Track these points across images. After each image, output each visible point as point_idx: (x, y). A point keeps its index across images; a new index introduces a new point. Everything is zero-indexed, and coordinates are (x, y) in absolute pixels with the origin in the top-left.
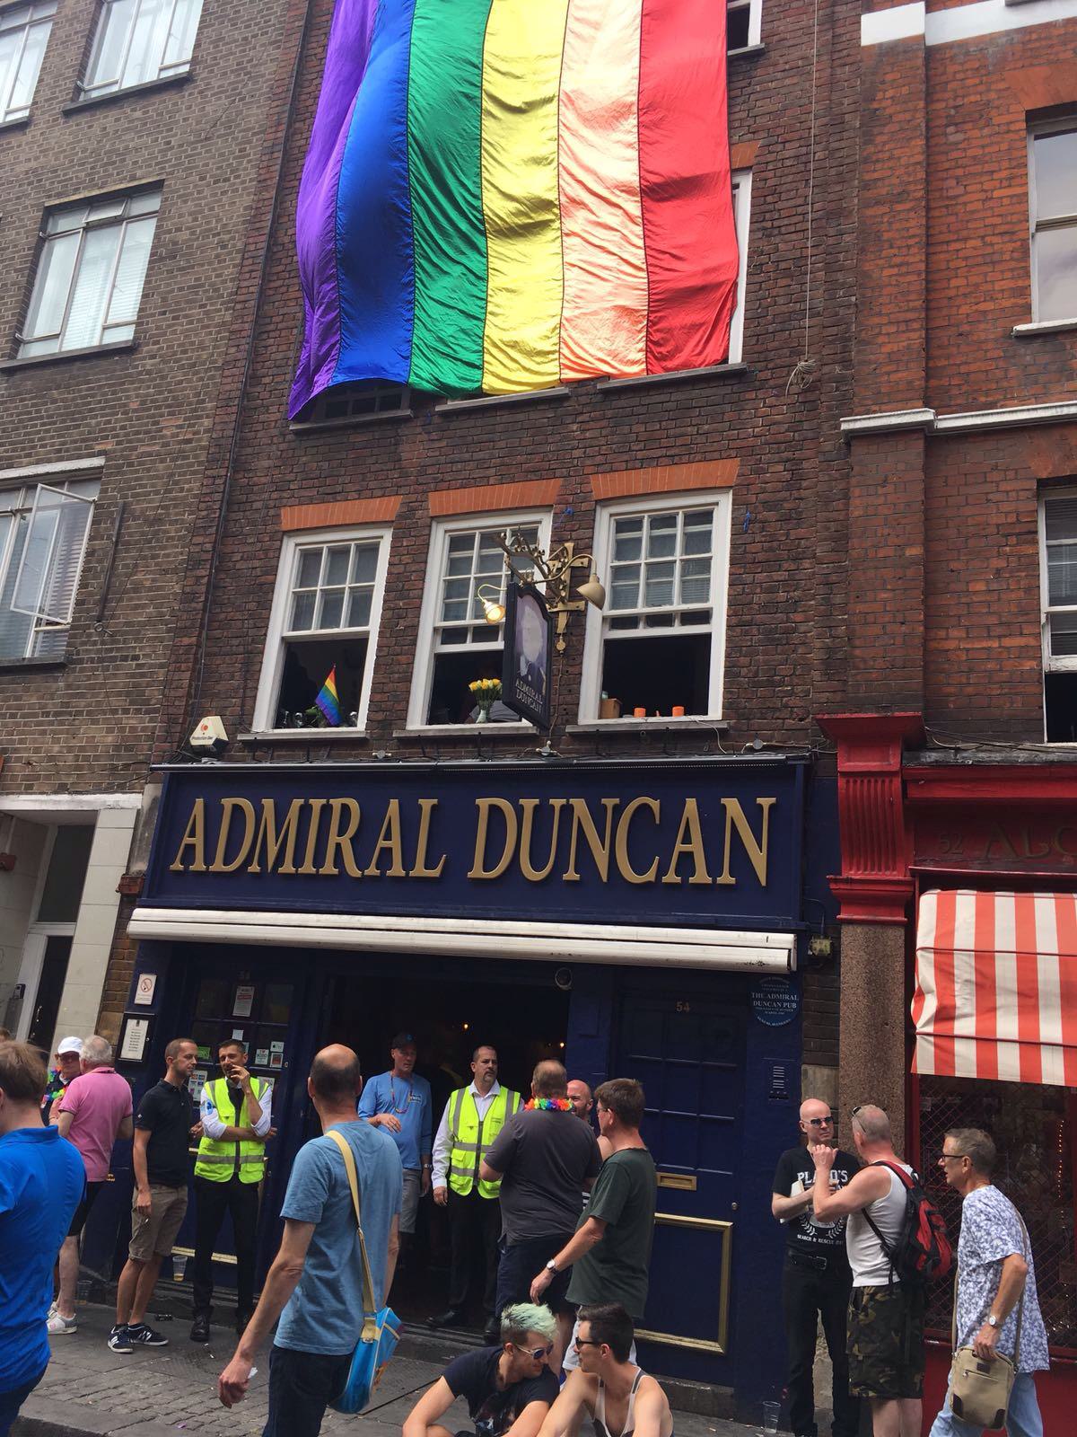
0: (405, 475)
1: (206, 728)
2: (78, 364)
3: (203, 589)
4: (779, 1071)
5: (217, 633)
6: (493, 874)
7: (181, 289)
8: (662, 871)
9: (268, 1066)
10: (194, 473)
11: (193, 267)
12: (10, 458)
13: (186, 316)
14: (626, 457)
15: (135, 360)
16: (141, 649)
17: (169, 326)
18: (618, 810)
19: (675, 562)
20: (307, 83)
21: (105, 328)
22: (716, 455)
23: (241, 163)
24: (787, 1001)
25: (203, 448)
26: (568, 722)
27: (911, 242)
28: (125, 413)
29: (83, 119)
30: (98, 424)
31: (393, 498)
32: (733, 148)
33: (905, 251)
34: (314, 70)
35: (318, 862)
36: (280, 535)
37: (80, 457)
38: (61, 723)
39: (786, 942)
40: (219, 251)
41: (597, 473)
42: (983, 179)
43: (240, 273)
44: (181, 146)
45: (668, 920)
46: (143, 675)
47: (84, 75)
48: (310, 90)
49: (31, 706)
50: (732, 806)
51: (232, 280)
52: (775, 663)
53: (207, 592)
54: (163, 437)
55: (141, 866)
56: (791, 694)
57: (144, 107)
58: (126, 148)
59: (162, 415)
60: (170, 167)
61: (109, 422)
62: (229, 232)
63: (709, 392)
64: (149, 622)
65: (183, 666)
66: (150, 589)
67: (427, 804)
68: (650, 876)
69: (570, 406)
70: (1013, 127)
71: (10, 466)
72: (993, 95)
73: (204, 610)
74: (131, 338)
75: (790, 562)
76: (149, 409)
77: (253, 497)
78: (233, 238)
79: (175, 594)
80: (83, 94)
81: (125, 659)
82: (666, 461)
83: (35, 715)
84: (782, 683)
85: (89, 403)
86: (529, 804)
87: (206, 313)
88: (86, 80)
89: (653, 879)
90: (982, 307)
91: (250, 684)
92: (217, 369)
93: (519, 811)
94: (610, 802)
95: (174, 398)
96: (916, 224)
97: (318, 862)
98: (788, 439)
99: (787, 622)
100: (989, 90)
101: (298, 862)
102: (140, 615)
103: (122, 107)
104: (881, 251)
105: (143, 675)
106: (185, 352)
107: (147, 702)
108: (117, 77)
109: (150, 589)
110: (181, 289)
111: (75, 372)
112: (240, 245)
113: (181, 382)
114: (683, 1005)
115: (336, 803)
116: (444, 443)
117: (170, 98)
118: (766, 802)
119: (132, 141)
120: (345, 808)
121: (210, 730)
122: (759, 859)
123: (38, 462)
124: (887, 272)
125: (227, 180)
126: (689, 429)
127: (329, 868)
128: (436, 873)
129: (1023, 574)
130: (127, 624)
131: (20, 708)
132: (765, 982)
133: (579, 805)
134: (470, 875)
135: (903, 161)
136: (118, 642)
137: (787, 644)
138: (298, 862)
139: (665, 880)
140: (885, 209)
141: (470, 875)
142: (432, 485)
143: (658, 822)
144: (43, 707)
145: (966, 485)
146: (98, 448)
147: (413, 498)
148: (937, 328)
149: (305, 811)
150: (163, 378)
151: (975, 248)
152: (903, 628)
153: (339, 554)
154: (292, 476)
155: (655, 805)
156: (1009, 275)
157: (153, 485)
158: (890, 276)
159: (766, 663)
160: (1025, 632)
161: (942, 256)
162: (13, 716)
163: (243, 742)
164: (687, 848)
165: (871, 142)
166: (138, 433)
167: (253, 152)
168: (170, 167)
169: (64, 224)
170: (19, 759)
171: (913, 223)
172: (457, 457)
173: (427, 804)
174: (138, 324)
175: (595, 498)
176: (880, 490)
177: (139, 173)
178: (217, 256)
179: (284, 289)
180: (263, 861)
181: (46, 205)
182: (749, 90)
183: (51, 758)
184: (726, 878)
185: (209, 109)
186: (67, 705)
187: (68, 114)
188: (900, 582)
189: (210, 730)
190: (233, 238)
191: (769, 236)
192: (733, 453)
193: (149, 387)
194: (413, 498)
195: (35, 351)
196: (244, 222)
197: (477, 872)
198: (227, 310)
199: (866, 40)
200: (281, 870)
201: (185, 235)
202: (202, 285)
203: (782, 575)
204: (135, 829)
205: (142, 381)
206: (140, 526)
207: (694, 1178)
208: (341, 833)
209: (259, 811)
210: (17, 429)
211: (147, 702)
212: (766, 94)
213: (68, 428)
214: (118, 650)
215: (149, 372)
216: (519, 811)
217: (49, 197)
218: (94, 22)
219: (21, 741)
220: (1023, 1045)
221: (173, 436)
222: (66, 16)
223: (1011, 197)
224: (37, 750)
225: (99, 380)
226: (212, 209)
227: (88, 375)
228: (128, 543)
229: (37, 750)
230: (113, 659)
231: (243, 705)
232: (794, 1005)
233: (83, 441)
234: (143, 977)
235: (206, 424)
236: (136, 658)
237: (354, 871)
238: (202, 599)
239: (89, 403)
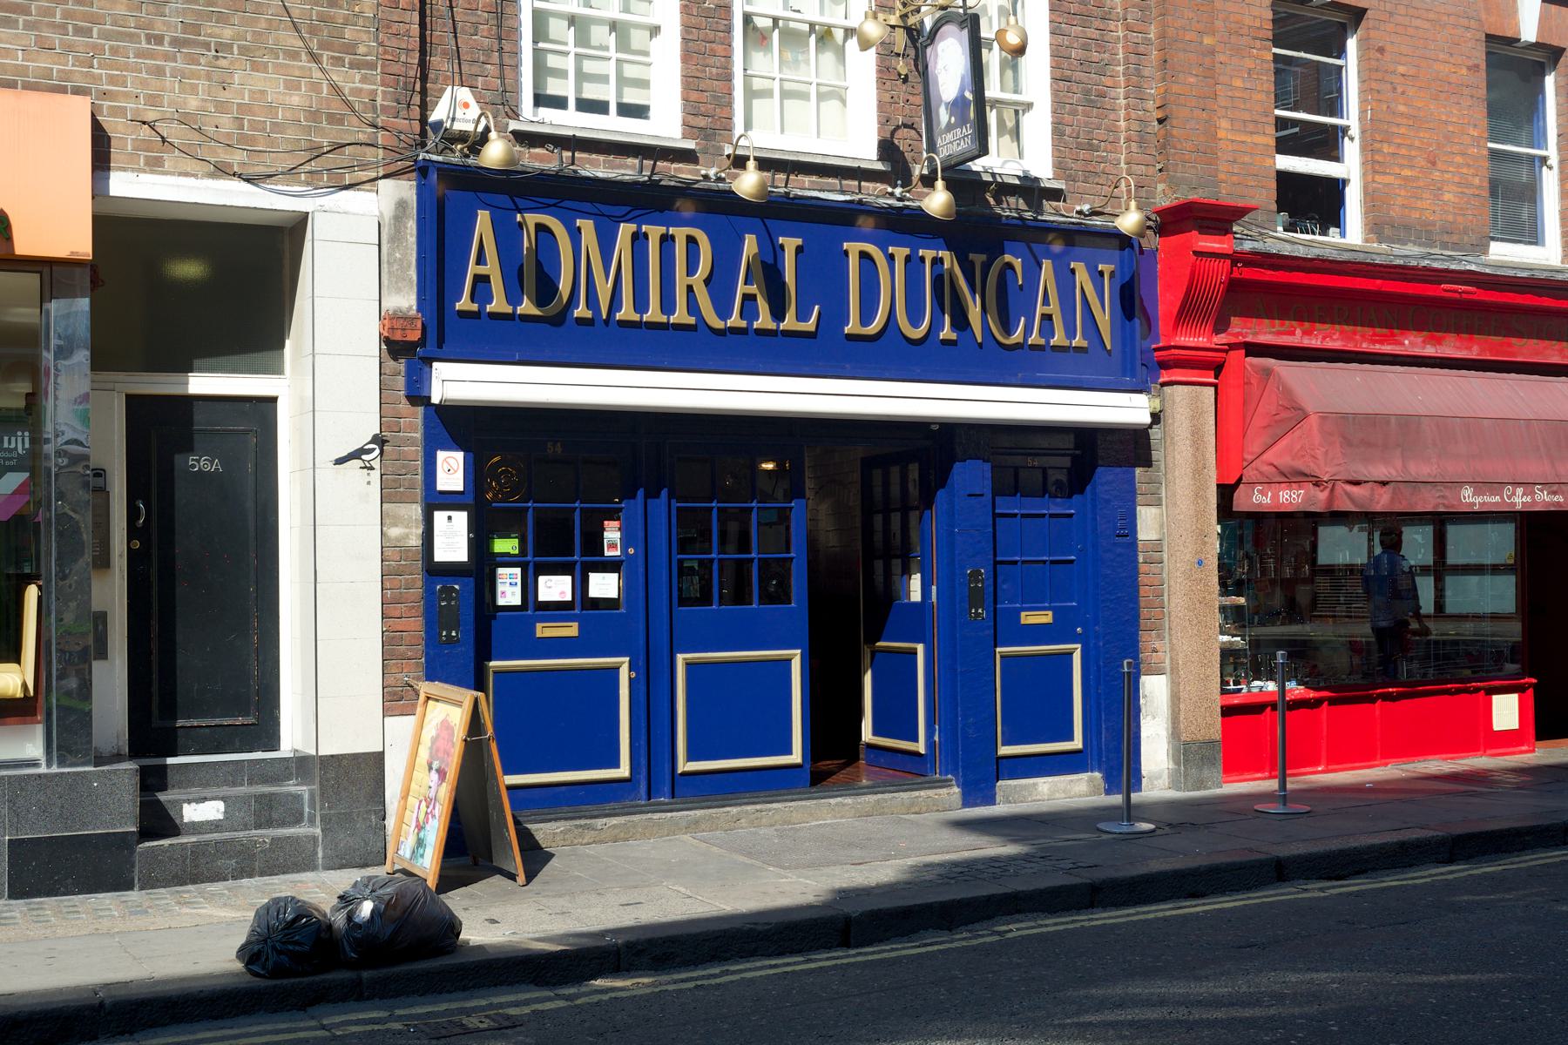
8: (1028, 330)
35: (667, 305)
52: (1093, 126)
86: (901, 253)
91: (507, 46)
93: (891, 258)
97: (667, 305)
101: (640, 303)
107: (350, 48)
120: (691, 240)
127: (680, 315)
128: (810, 325)
138: (640, 303)
160: (808, 25)
164: (482, 270)
170: (122, 112)
173: (790, 244)
180: (592, 301)
184: (1078, 341)
186: (196, 28)
197: (852, 326)
200: (618, 316)
207: (1050, 613)
209: (575, 234)
211: (350, 48)
231: (502, 77)
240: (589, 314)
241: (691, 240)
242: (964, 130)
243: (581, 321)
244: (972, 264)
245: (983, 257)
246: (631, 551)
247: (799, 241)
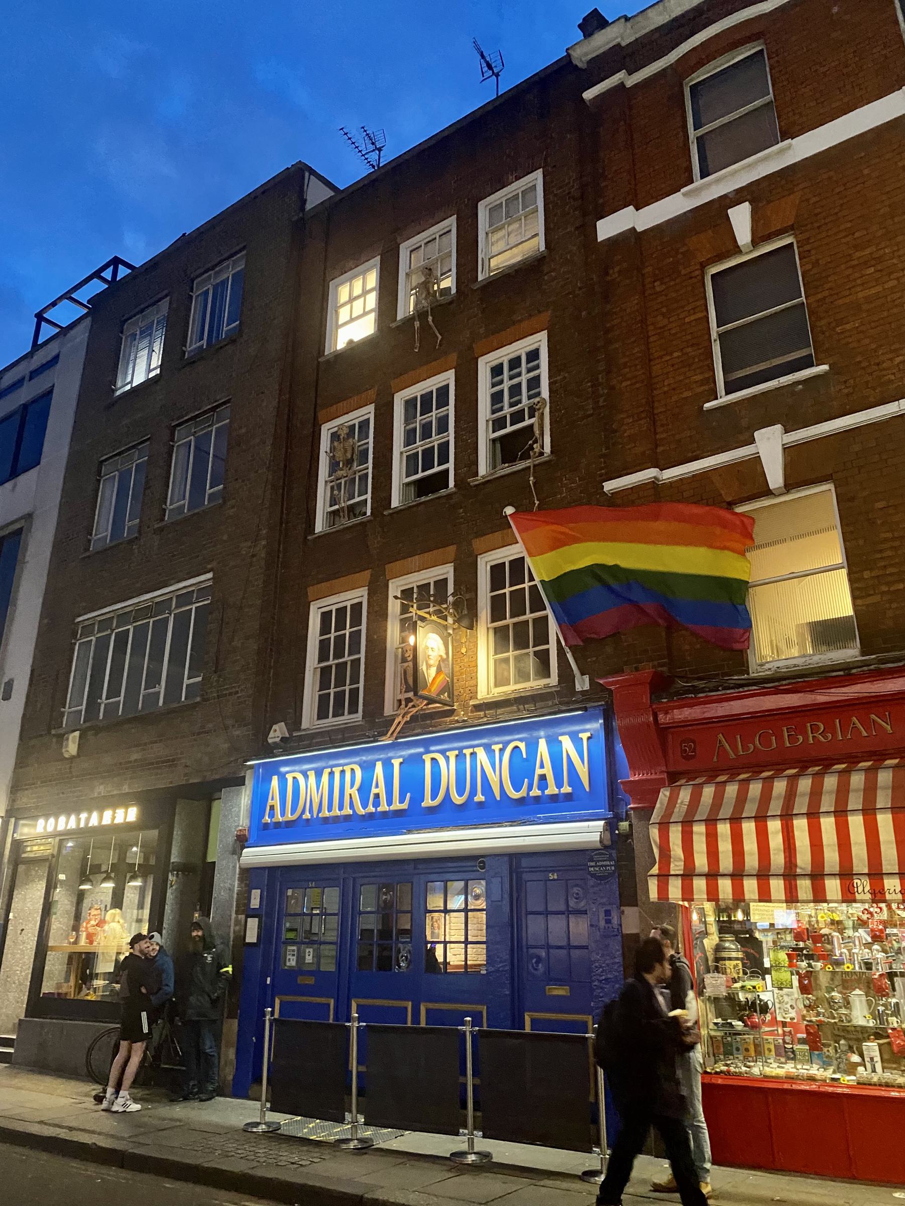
1: (275, 731)
6: (436, 802)
8: (530, 788)
18: (502, 751)
24: (608, 866)
26: (471, 698)
27: (637, 362)
32: (66, 302)
33: (633, 368)
39: (599, 826)
42: (679, 311)
70: (693, 275)
72: (680, 256)
81: (230, 694)
89: (525, 795)
114: (553, 875)
120: (352, 770)
124: (624, 384)
127: (348, 811)
128: (404, 806)
132: (596, 855)
134: (423, 805)
135: (628, 311)
139: (532, 794)
141: (423, 805)
146: (209, 566)
155: (522, 746)
156: (698, 371)
158: (626, 386)
171: (636, 350)
180: (311, 811)
184: (567, 789)
197: (428, 802)
199: (601, 237)
200: (320, 815)
201: (243, 430)
219: (182, 753)
220: (710, 878)
223: (696, 320)
232: (613, 868)
234: (254, 891)
241: (352, 770)
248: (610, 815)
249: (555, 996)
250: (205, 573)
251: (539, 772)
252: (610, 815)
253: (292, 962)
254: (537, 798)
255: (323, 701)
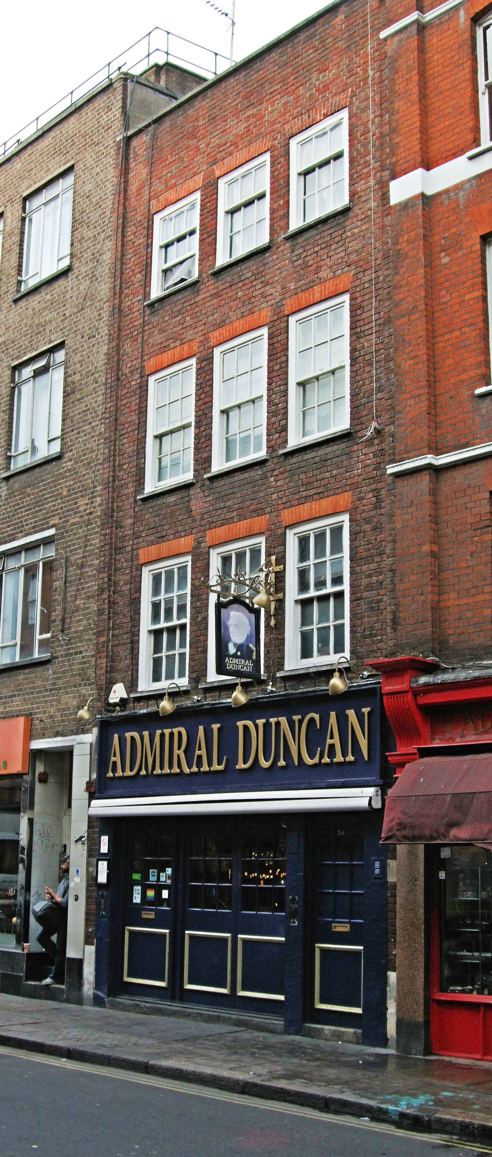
0: (194, 521)
1: (115, 692)
2: (37, 470)
3: (106, 606)
4: (377, 864)
5: (117, 632)
6: (133, 773)
7: (79, 414)
8: (321, 757)
9: (166, 881)
10: (96, 533)
11: (83, 398)
12: (13, 534)
13: (83, 431)
14: (297, 497)
15: (63, 463)
16: (83, 646)
17: (76, 439)
18: (301, 722)
19: (326, 561)
20: (128, 261)
21: (50, 441)
22: (340, 490)
23: (99, 324)
25: (98, 517)
28: (61, 499)
29: (23, 303)
30: (50, 507)
31: (190, 536)
34: (131, 251)
36: (140, 566)
37: (44, 530)
38: (53, 695)
40: (95, 385)
41: (285, 508)
43: (106, 399)
44: (71, 316)
45: (323, 785)
46: (85, 663)
47: (21, 271)
48: (129, 266)
49: (39, 687)
50: (351, 713)
51: (103, 404)
53: (109, 607)
54: (80, 512)
55: (94, 776)
56: (381, 641)
57: (50, 292)
58: (45, 321)
59: (78, 498)
60: (67, 331)
61: (54, 506)
62: (98, 372)
63: (335, 448)
64: (85, 630)
65: (102, 655)
66: (83, 610)
67: (215, 727)
68: (316, 760)
69: (270, 465)
71: (14, 540)
73: (109, 619)
74: (59, 450)
75: (378, 557)
76: (71, 495)
77: (126, 544)
78: (100, 376)
79: (94, 611)
80: (23, 283)
81: (76, 653)
82: (316, 496)
83: (41, 692)
84: (376, 635)
85: (44, 495)
86: (261, 722)
87: (92, 428)
88: (23, 273)
90: (461, 378)
92: (100, 464)
93: (256, 726)
94: (296, 718)
95: (83, 486)
96: (421, 328)
98: (374, 476)
99: (378, 596)
100: (461, 223)
101: (162, 768)
102: (80, 625)
103: (40, 293)
104: (405, 349)
105: (85, 663)
106: (84, 455)
108: (38, 270)
109: (83, 610)
110: (79, 414)
111: (36, 475)
112: (104, 380)
113: (84, 475)
115: (175, 730)
116: (211, 498)
117: (61, 282)
118: (366, 710)
119: (48, 316)
120: (180, 733)
121: (118, 692)
122: (363, 743)
123: (26, 535)
125: (94, 336)
126: (327, 474)
128: (221, 767)
129: (484, 554)
130: (75, 632)
131: (34, 688)
133: (283, 720)
136: (71, 644)
137: (378, 609)
138: (162, 768)
139: (323, 761)
140: (405, 319)
142: (208, 526)
143: (318, 727)
144: (44, 686)
145: (456, 498)
146: (52, 523)
147: (199, 535)
148: (441, 394)
149: (162, 735)
150: (76, 473)
151: (457, 337)
152: (423, 597)
153: (170, 574)
154: (142, 529)
155: (317, 717)
157: (79, 544)
159: (369, 622)
161: (441, 344)
162: (32, 693)
163: (134, 698)
165: (397, 273)
166: (68, 511)
167: (105, 315)
168: (67, 331)
169: (27, 372)
172: (217, 506)
173: (215, 727)
174: (63, 438)
175: (284, 525)
176: (410, 510)
177: (53, 338)
178: (94, 389)
179: (128, 405)
181: (12, 365)
182: (344, 236)
183: (51, 717)
184: (350, 758)
185: (82, 288)
187: (16, 301)
188: (420, 568)
189: (118, 692)
190: (100, 376)
191: (359, 338)
192: (348, 488)
193: (70, 480)
194: (199, 535)
195: (21, 463)
196: (105, 364)
197: (241, 765)
198: (101, 424)
200: (154, 772)
202: (89, 410)
203: (373, 566)
204: (91, 754)
205: (67, 477)
206: (74, 570)
208: (179, 749)
209: (142, 738)
210: (14, 515)
212: (354, 237)
213: (37, 512)
214: (73, 648)
215: (69, 471)
216: (256, 726)
217: (13, 360)
218: (22, 233)
219: (38, 708)
221: (85, 510)
222: (8, 232)
224: (45, 712)
225: (47, 479)
226: (89, 358)
227: (42, 476)
228: (70, 582)
229: (45, 712)
230: (71, 654)
233: (45, 519)
235: (98, 501)
236: (81, 652)
237: (187, 770)
238: (107, 613)
239: (44, 495)
240: (178, 771)
242: (247, 662)
243: (144, 776)
244: (294, 721)
245: (300, 717)
246: (271, 871)
247: (219, 725)
248: (381, 782)
249: (337, 932)
250: (49, 528)
251: (198, 752)
252: (381, 782)
253: (137, 899)
254: (327, 764)
255: (306, 639)
